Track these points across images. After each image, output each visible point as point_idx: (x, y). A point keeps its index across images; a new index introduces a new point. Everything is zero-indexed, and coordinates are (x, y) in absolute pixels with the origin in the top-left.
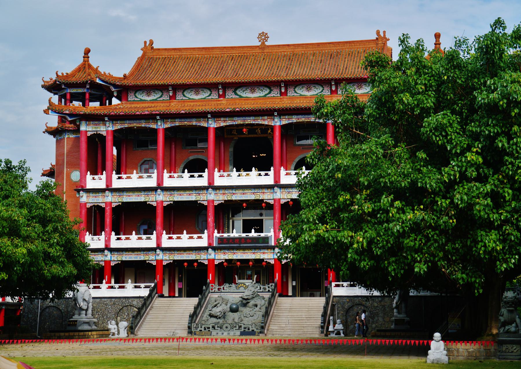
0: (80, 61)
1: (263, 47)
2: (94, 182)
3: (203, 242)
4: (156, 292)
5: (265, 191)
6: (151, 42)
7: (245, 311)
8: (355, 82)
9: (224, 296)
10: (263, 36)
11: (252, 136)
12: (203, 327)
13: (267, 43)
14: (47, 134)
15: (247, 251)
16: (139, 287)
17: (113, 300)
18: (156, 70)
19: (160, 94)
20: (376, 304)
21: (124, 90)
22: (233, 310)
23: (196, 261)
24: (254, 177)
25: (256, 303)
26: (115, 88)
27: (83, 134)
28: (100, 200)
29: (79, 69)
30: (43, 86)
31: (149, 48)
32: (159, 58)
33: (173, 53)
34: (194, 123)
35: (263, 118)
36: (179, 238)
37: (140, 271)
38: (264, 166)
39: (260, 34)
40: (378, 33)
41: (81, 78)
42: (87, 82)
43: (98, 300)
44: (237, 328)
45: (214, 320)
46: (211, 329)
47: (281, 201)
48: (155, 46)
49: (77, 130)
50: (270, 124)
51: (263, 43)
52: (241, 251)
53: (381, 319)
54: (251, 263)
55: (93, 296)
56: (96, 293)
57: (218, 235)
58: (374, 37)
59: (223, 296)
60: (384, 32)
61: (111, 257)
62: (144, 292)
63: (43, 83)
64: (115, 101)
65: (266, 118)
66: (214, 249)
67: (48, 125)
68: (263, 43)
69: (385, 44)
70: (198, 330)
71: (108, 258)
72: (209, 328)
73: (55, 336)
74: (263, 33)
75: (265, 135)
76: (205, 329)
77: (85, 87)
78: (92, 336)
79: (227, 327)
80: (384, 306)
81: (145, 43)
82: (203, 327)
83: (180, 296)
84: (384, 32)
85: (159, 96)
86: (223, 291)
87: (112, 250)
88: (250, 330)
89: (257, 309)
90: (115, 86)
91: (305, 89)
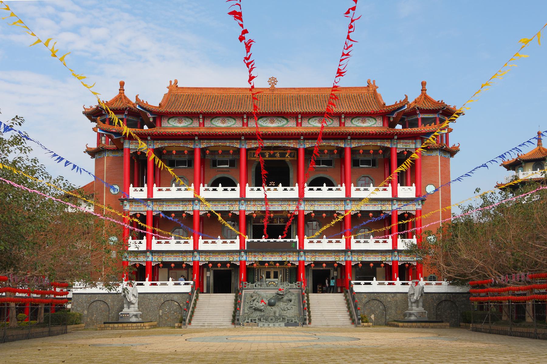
0: (116, 93)
1: (273, 89)
2: (135, 193)
3: (236, 246)
4: (199, 288)
5: (291, 203)
6: (176, 82)
7: (281, 305)
8: (360, 117)
9: (265, 291)
10: (273, 81)
11: (272, 159)
12: (250, 319)
13: (276, 86)
14: (87, 154)
15: (275, 254)
16: (179, 284)
17: (156, 295)
18: (184, 104)
19: (191, 121)
20: (389, 300)
21: (160, 115)
22: (271, 305)
23: (229, 262)
24: (279, 192)
25: (290, 298)
26: (151, 115)
27: (127, 152)
28: (142, 209)
29: (116, 99)
30: (84, 113)
31: (174, 88)
32: (184, 95)
33: (195, 91)
34: (228, 144)
35: (289, 141)
36: (213, 242)
37: (175, 269)
38: (286, 183)
39: (273, 78)
40: (369, 82)
41: (119, 105)
42: (126, 108)
43: (142, 295)
44: (281, 320)
45: (258, 313)
46: (257, 321)
47: (305, 212)
48: (179, 85)
49: (119, 148)
50: (295, 147)
51: (273, 86)
52: (270, 254)
53: (393, 312)
54: (372, 265)
55: (139, 292)
56: (141, 289)
57: (249, 240)
58: (366, 85)
59: (258, 292)
60: (374, 81)
61: (152, 258)
62: (187, 289)
63: (84, 110)
64: (146, 127)
65: (292, 141)
66: (246, 252)
67: (88, 146)
68: (273, 86)
69: (375, 91)
70: (246, 321)
71: (150, 259)
72: (255, 320)
73: (109, 327)
74: (270, 79)
75: (283, 159)
76: (251, 321)
77: (123, 113)
78: (144, 328)
79: (272, 319)
80: (396, 301)
81: (171, 82)
82: (250, 319)
83: (208, 292)
84: (374, 81)
85: (189, 123)
86: (255, 288)
87: (153, 252)
88: (293, 322)
89: (292, 303)
90: (151, 112)
91: (177, 121)
